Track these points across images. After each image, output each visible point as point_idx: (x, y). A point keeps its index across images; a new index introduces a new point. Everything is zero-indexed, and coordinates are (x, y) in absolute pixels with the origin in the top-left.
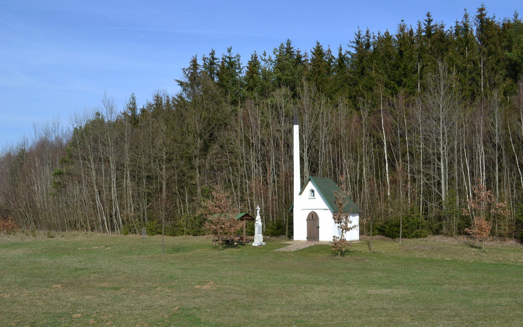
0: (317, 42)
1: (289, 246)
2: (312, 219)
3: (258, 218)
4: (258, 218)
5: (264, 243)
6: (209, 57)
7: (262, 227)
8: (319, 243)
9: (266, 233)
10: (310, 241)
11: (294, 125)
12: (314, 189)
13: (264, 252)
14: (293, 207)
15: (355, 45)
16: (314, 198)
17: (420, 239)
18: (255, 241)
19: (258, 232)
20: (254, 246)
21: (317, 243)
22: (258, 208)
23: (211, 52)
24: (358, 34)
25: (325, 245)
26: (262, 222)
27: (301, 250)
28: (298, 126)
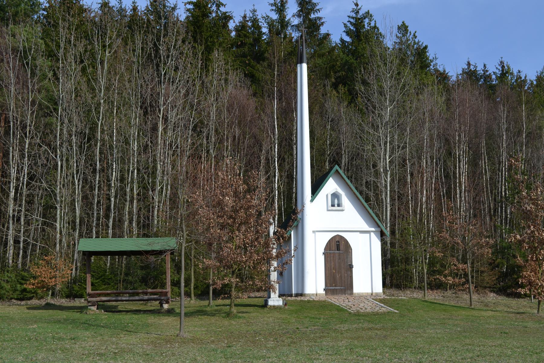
20: (274, 306)
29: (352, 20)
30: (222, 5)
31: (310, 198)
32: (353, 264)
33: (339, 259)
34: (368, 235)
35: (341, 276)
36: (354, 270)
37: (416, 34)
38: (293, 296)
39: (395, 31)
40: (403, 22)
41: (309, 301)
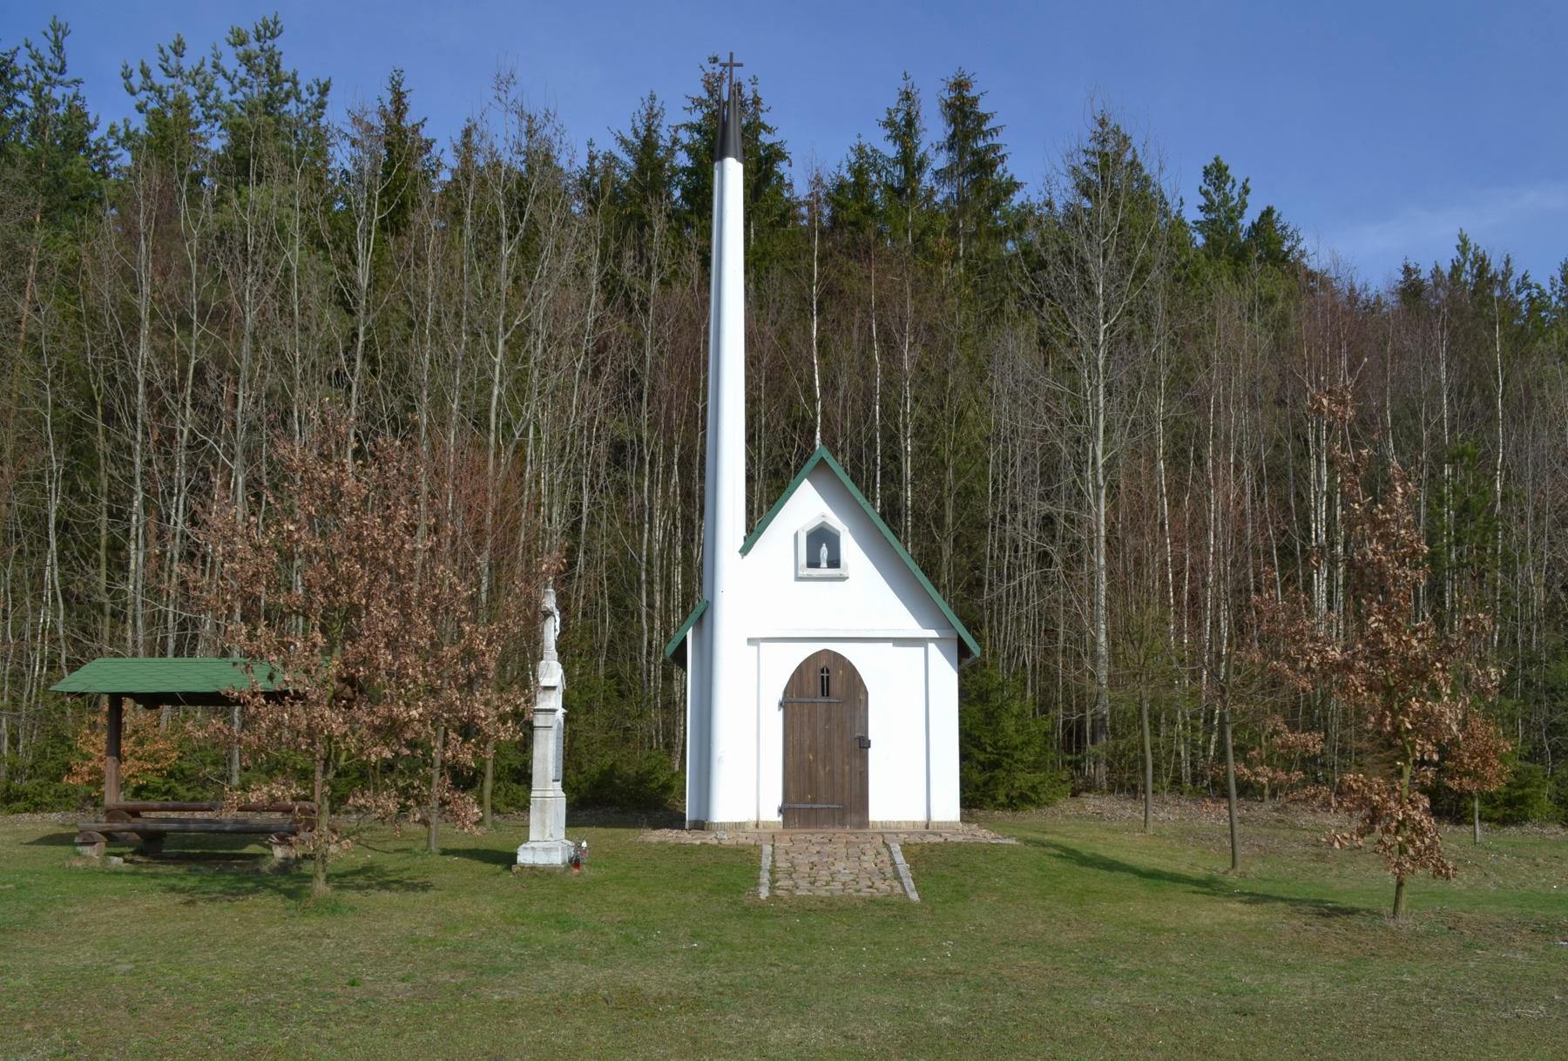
12: (836, 522)
20: (533, 868)
29: (1093, 160)
30: (765, 127)
31: (742, 543)
32: (873, 734)
33: (829, 720)
34: (922, 650)
35: (832, 773)
36: (873, 754)
37: (1249, 185)
38: (687, 826)
39: (1199, 179)
40: (1216, 159)
41: (718, 849)
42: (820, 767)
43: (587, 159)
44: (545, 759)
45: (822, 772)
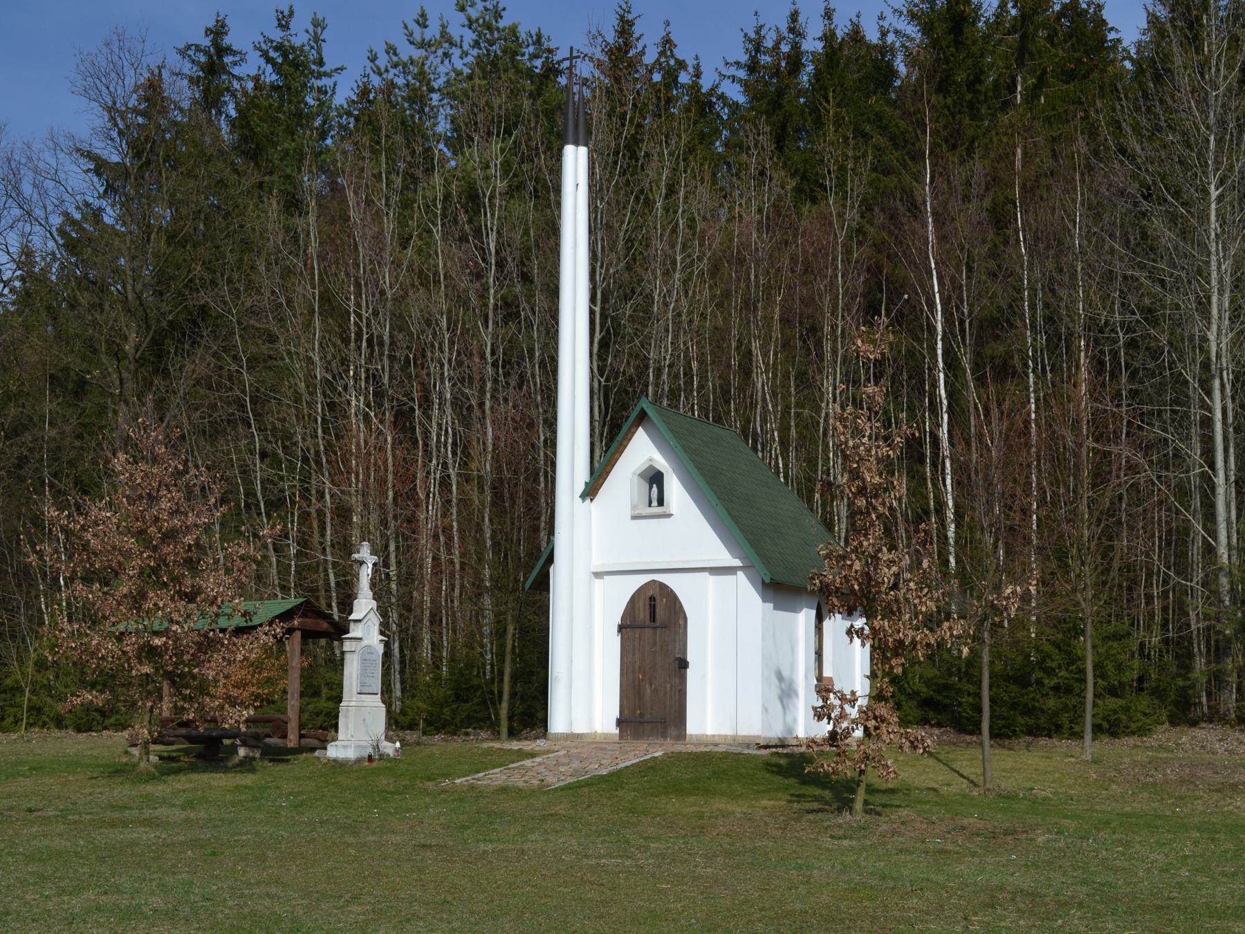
0: (622, 17)
1: (527, 763)
2: (648, 622)
3: (364, 605)
4: (364, 605)
5: (390, 748)
6: (206, 42)
7: (387, 655)
8: (691, 748)
9: (401, 719)
10: (637, 735)
11: (568, 143)
12: (662, 463)
13: (391, 788)
14: (550, 560)
15: (742, 74)
16: (660, 510)
17: (1125, 740)
18: (341, 735)
19: (363, 685)
20: (335, 760)
21: (679, 747)
22: (365, 553)
23: (211, 24)
24: (753, 35)
25: (726, 755)
26: (384, 629)
27: (602, 778)
28: (583, 151)
42: (648, 686)
43: (878, 35)
44: (351, 677)
45: (649, 690)
